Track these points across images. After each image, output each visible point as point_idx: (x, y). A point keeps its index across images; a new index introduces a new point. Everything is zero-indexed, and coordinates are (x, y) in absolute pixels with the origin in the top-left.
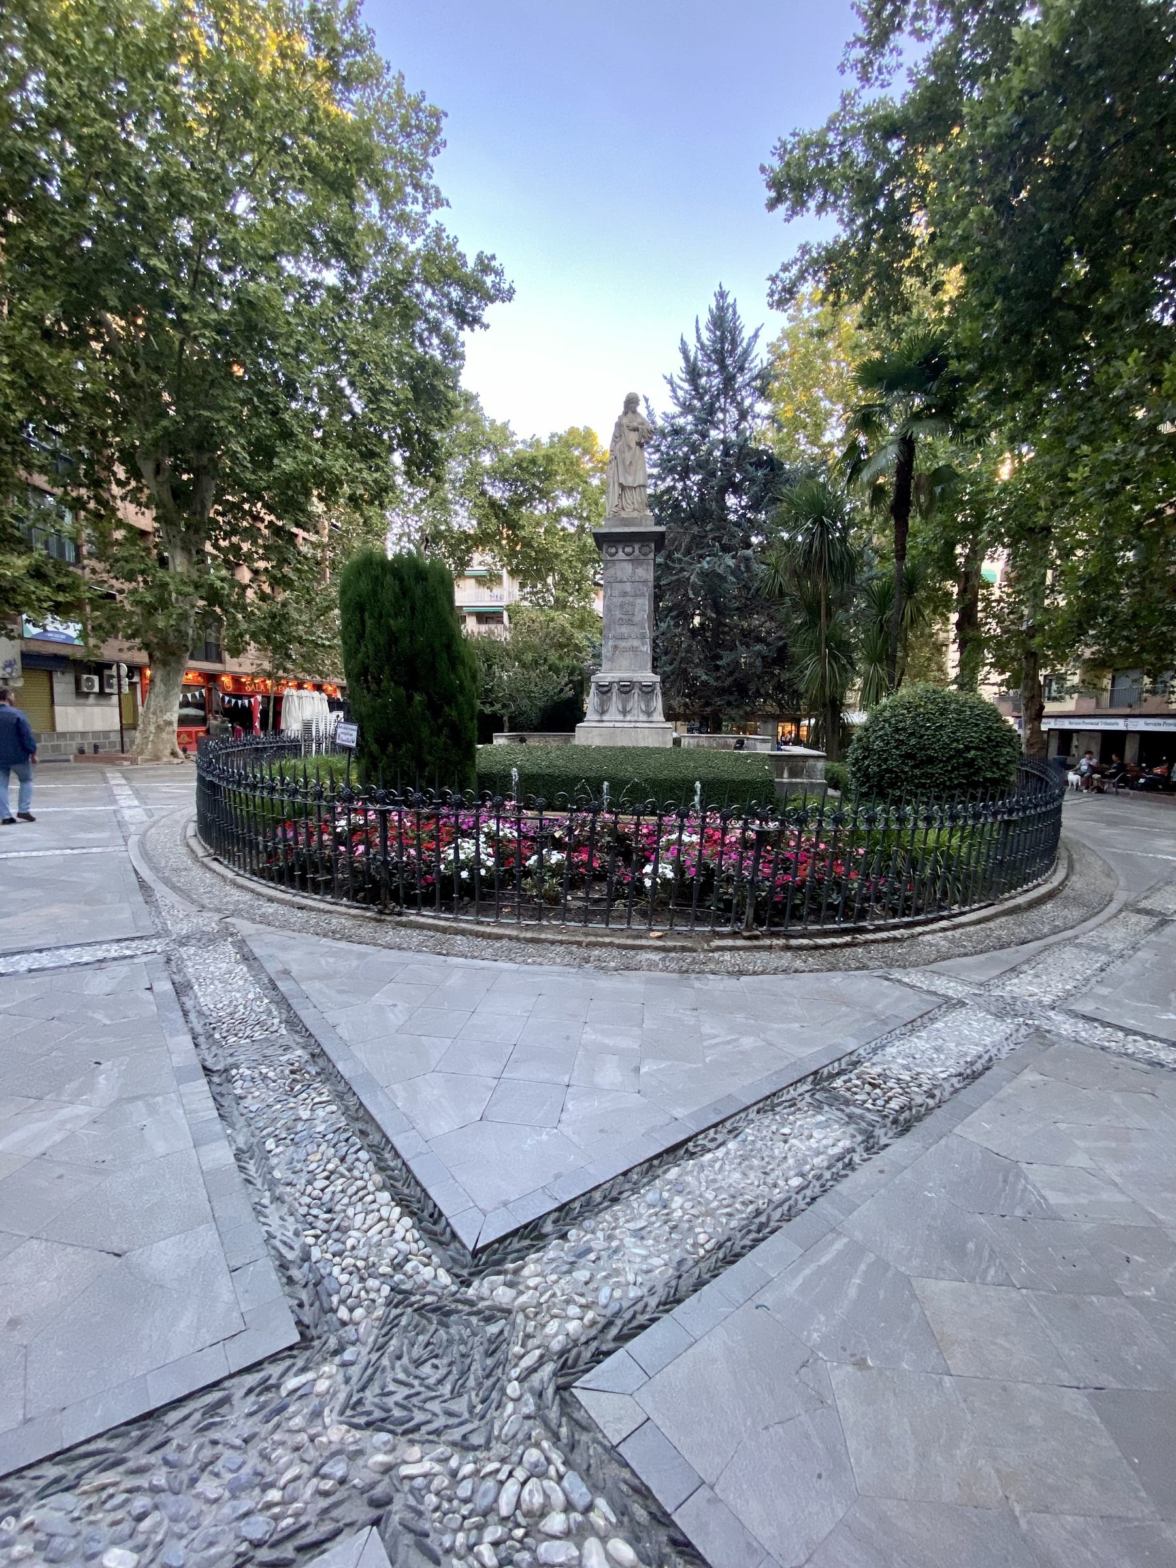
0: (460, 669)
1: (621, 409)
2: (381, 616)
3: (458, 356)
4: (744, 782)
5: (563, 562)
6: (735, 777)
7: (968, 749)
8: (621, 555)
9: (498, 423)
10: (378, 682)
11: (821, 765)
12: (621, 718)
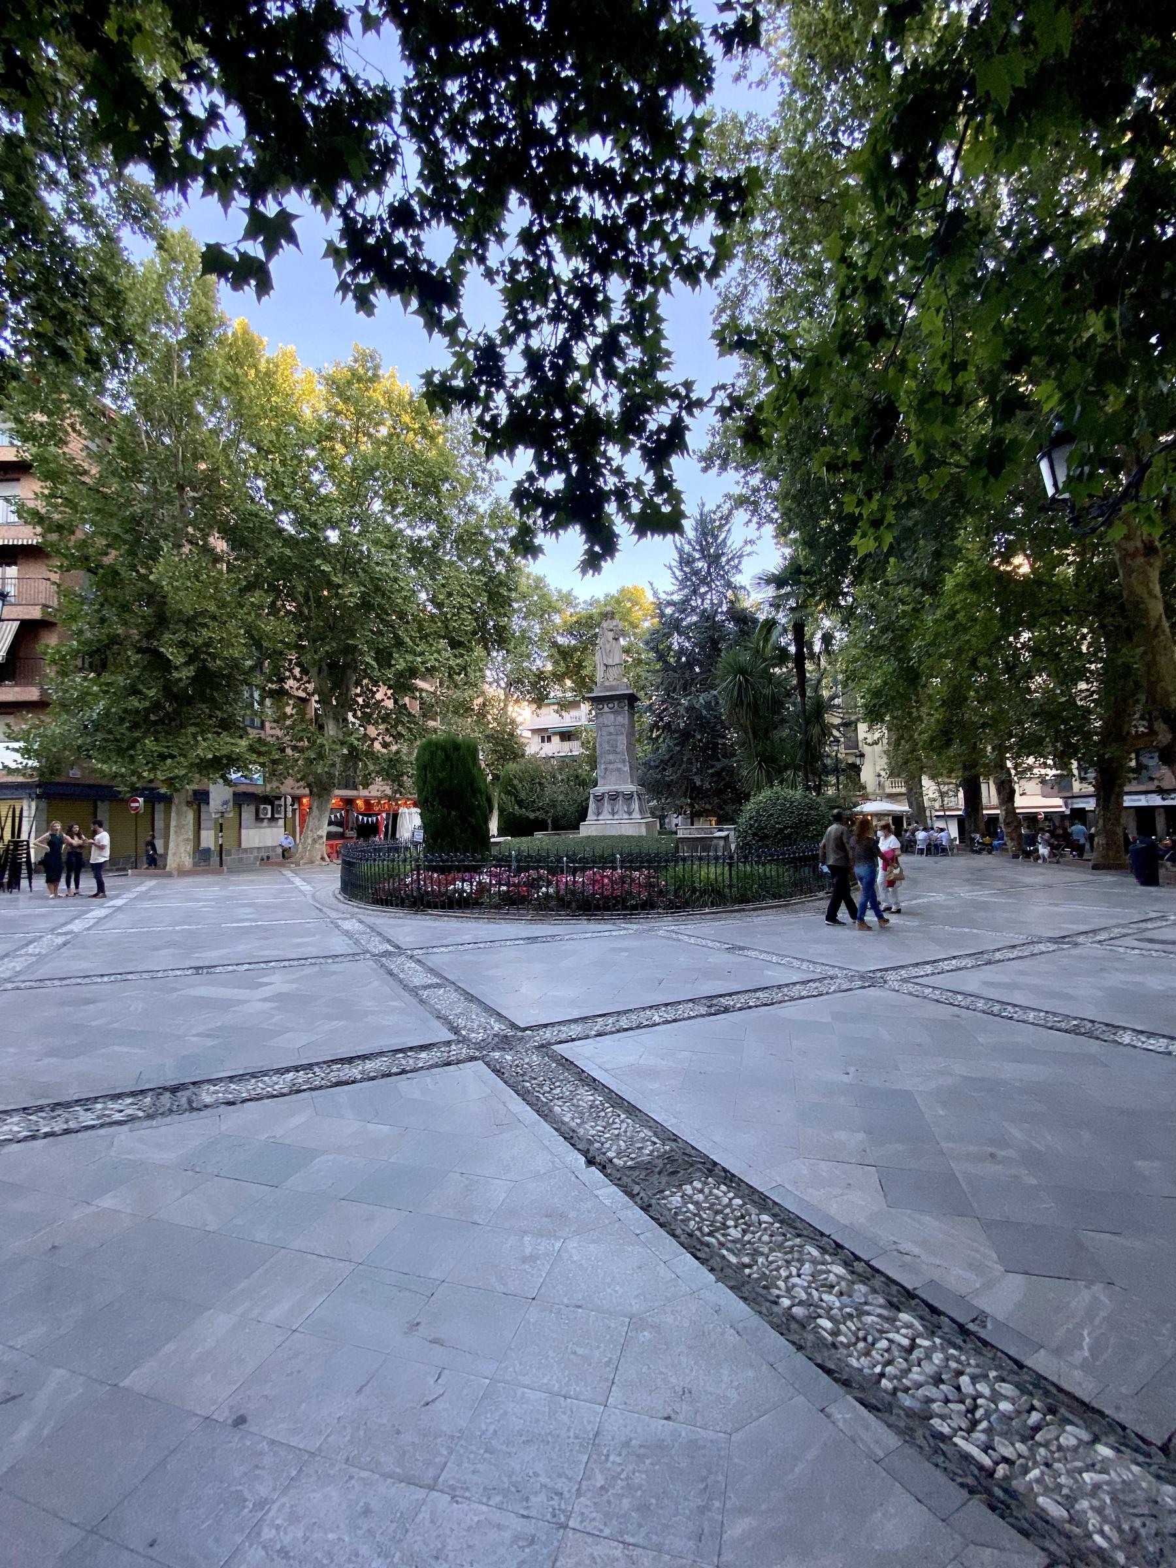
7: (786, 828)
8: (606, 709)
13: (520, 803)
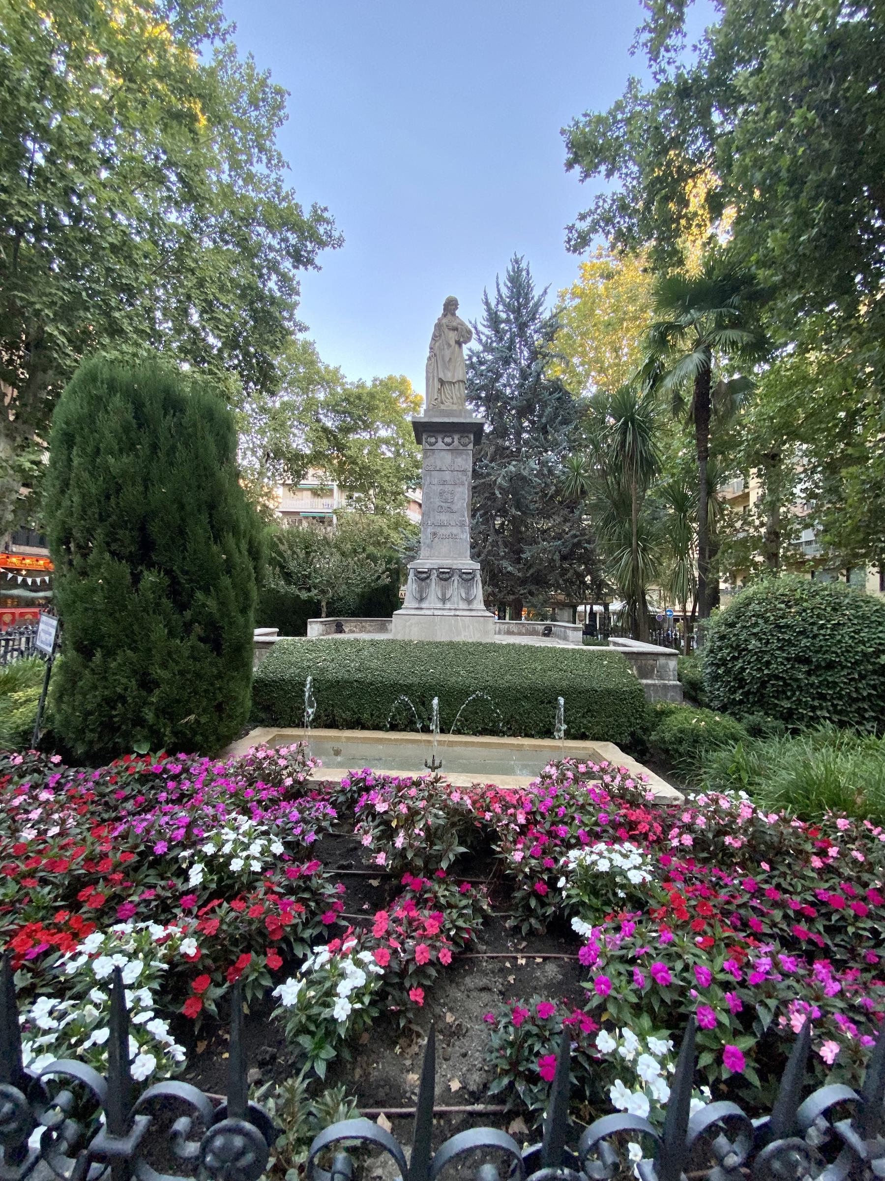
0: (230, 540)
2: (97, 451)
3: (294, 291)
4: (609, 692)
5: (381, 477)
6: (595, 685)
8: (440, 445)
9: (331, 368)
10: (84, 551)
11: (673, 664)
12: (440, 605)
13: (288, 576)
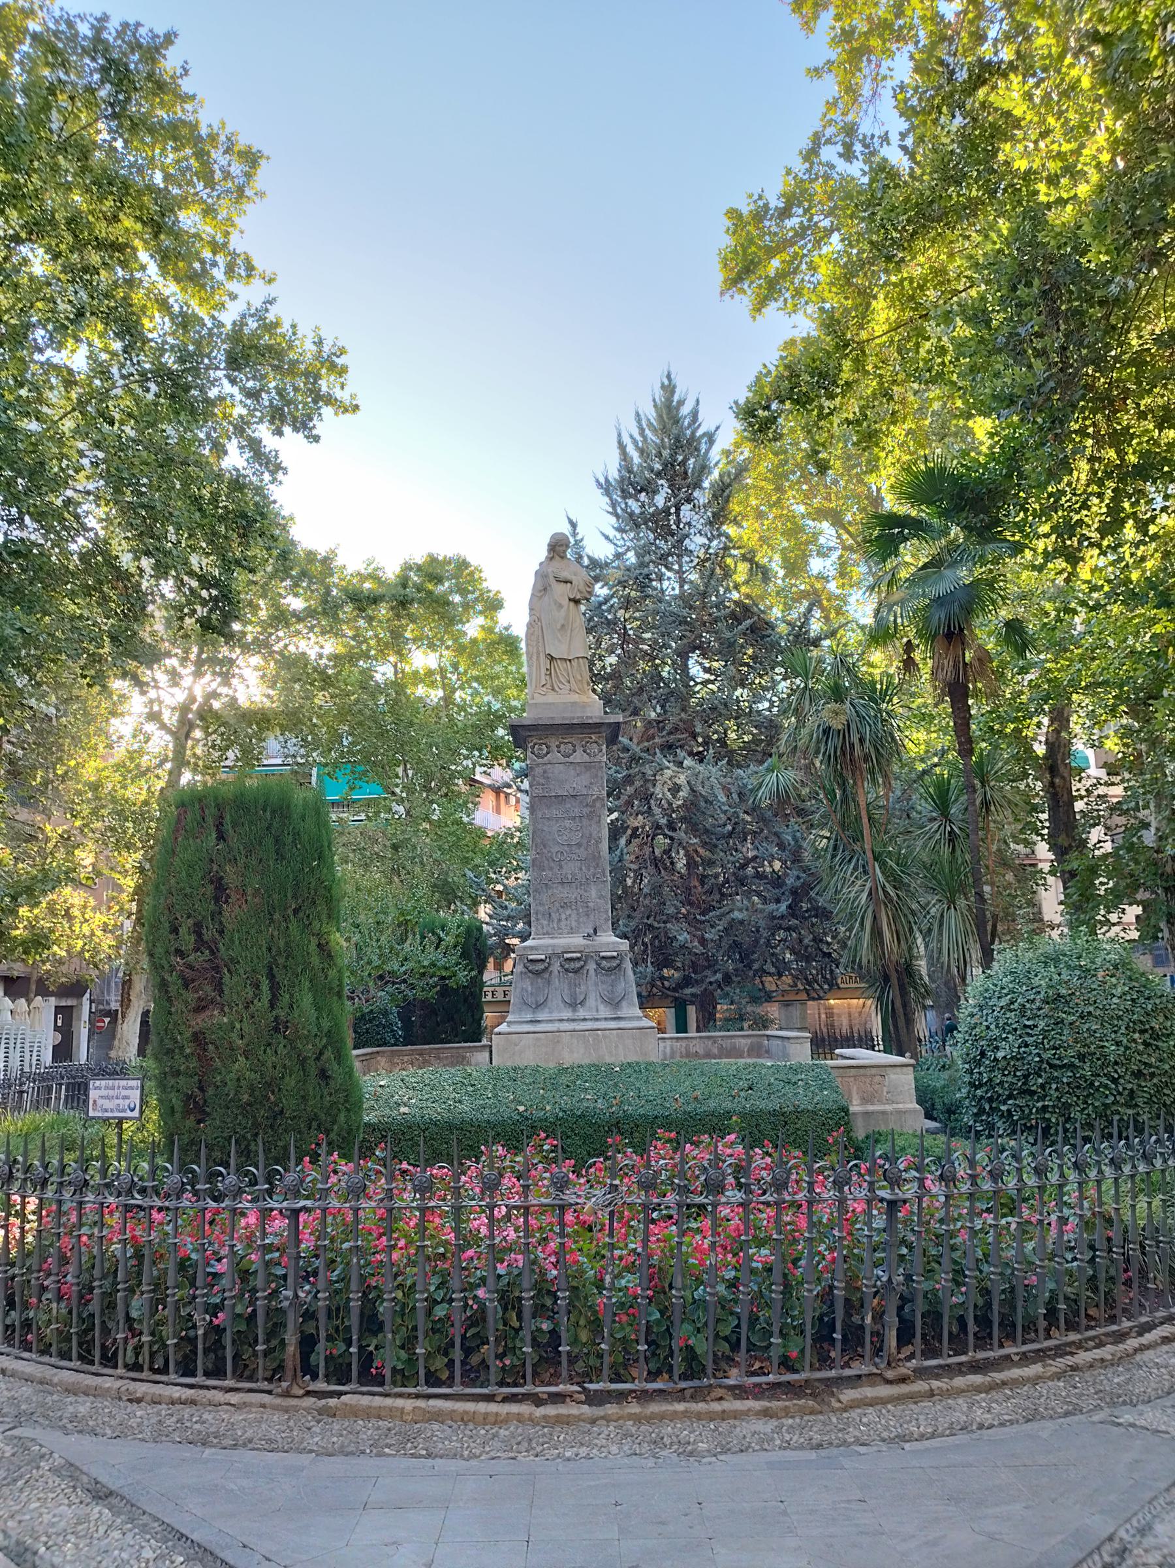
1: (542, 553)
